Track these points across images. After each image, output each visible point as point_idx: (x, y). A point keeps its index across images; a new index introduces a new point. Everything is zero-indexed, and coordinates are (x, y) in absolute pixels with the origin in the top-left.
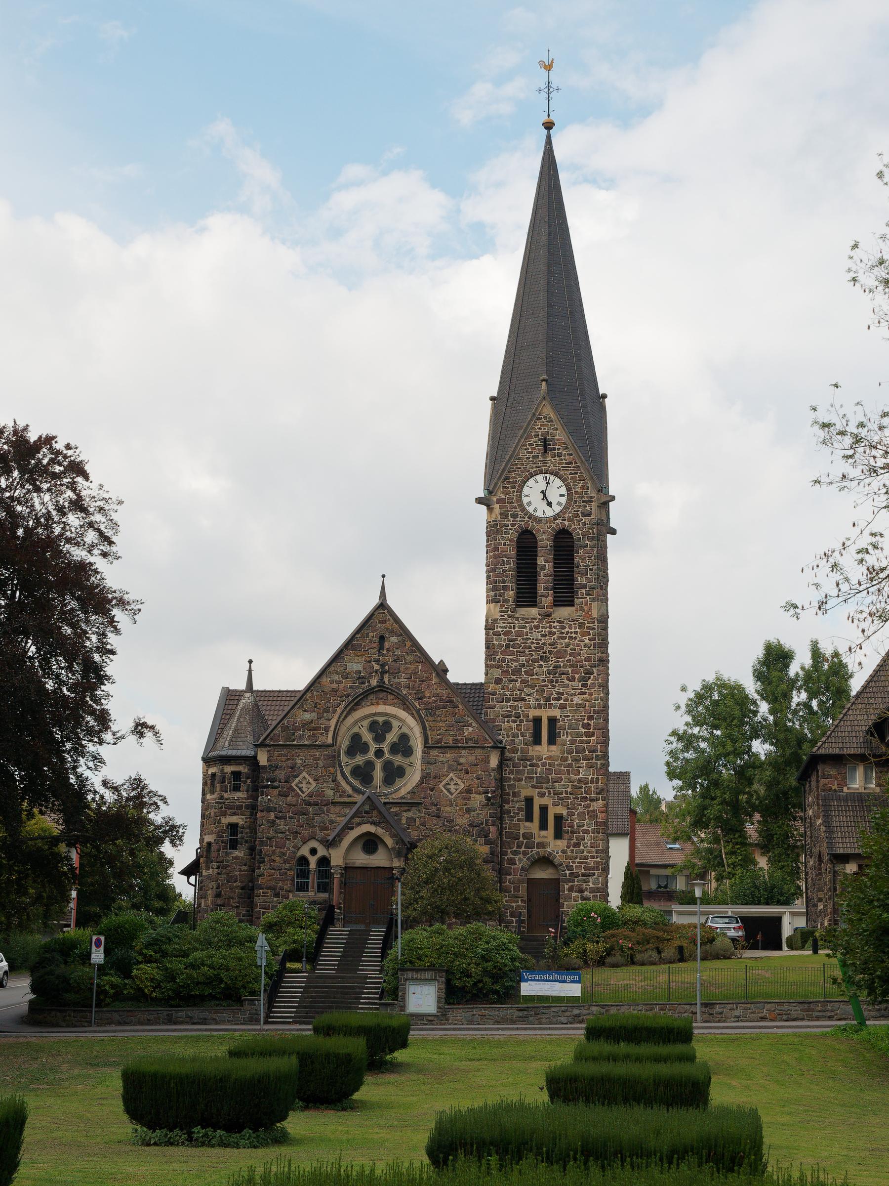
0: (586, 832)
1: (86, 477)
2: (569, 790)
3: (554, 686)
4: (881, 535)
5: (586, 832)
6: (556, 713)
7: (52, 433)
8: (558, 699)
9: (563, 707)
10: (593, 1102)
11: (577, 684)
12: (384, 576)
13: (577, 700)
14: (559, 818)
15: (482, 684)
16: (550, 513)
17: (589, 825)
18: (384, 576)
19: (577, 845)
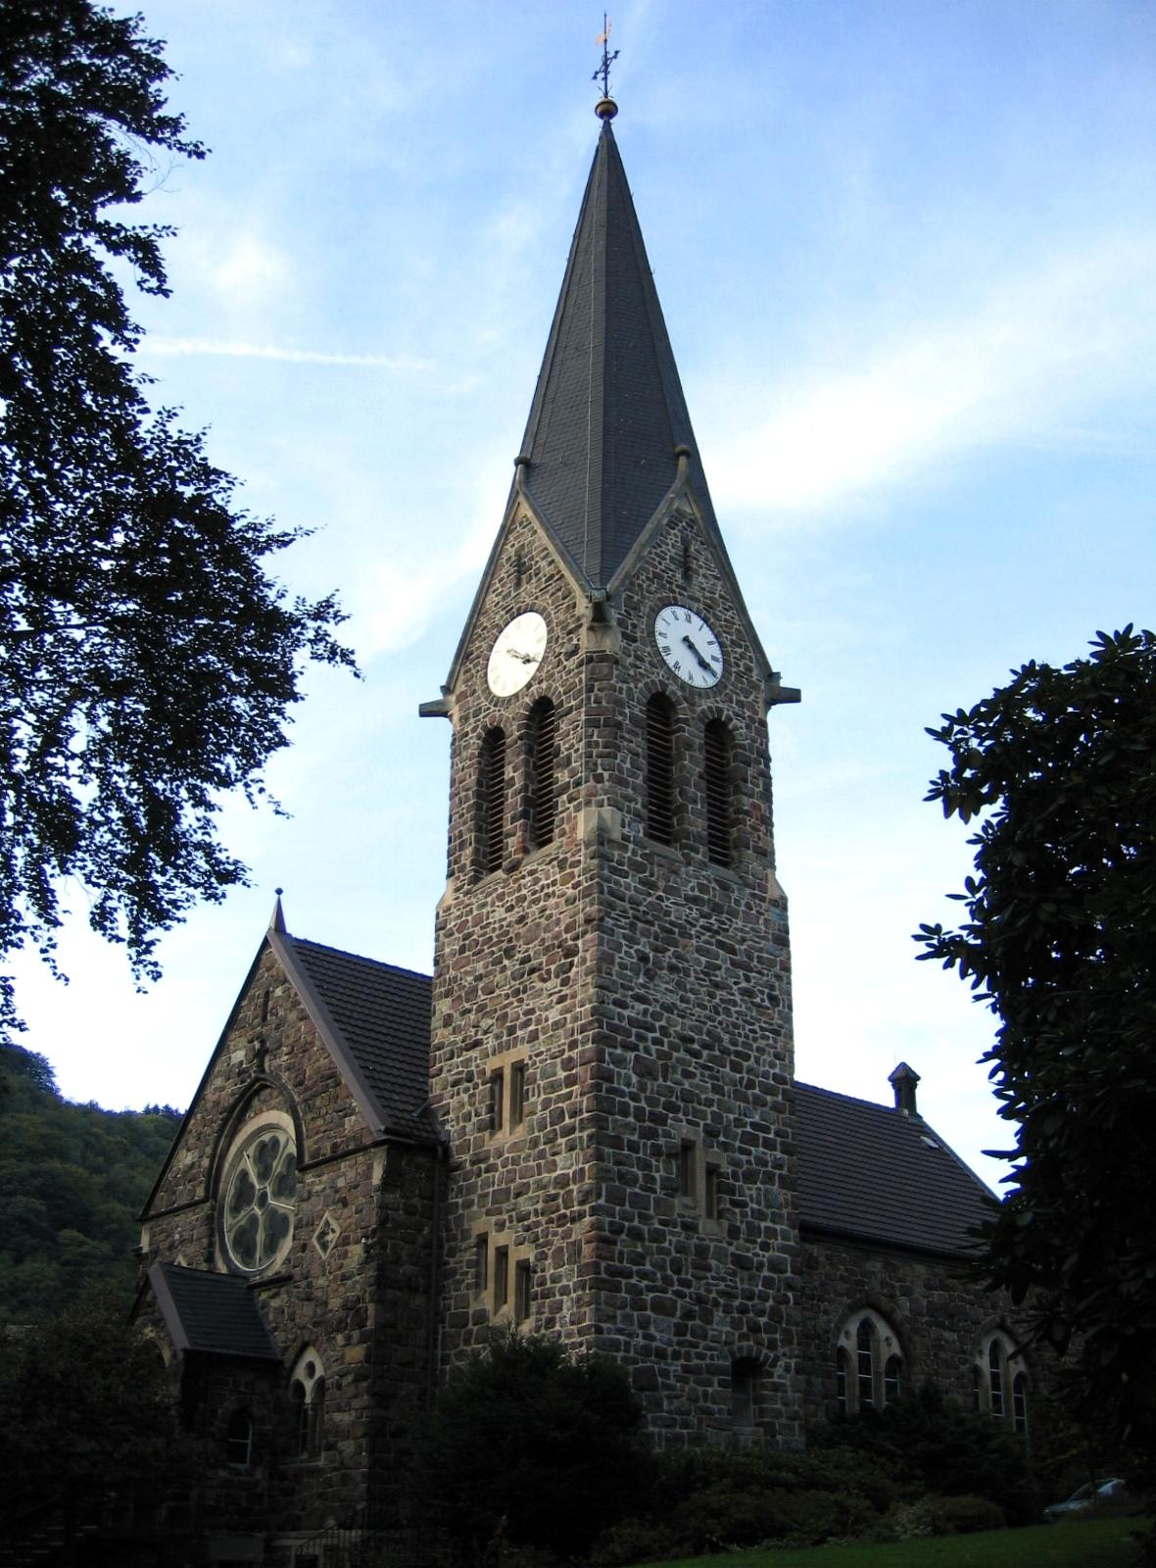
0: (565, 1291)
1: (79, 803)
2: (540, 1206)
3: (521, 1001)
4: (262, 781)
5: (565, 1291)
6: (523, 1052)
7: (924, 732)
8: (526, 1024)
9: (533, 1037)
10: (527, 726)
11: (553, 983)
12: (279, 892)
13: (554, 1015)
14: (524, 1268)
15: (431, 978)
16: (711, 682)
17: (569, 1277)
18: (279, 892)
19: (550, 1322)
